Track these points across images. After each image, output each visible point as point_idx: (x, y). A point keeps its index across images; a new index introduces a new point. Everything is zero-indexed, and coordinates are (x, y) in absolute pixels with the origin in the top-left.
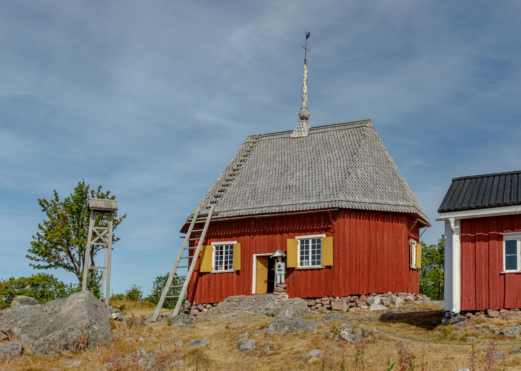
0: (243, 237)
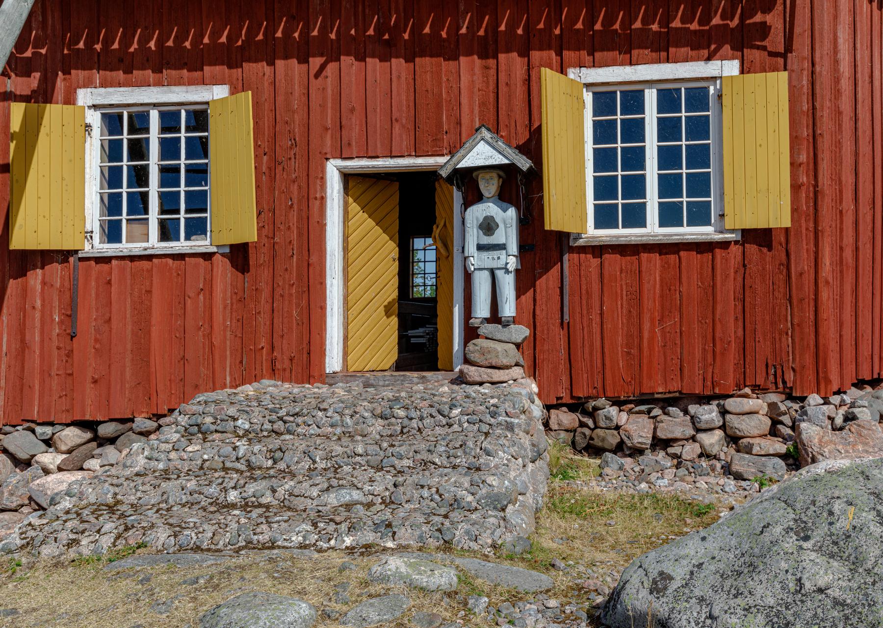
0: (263, 67)
